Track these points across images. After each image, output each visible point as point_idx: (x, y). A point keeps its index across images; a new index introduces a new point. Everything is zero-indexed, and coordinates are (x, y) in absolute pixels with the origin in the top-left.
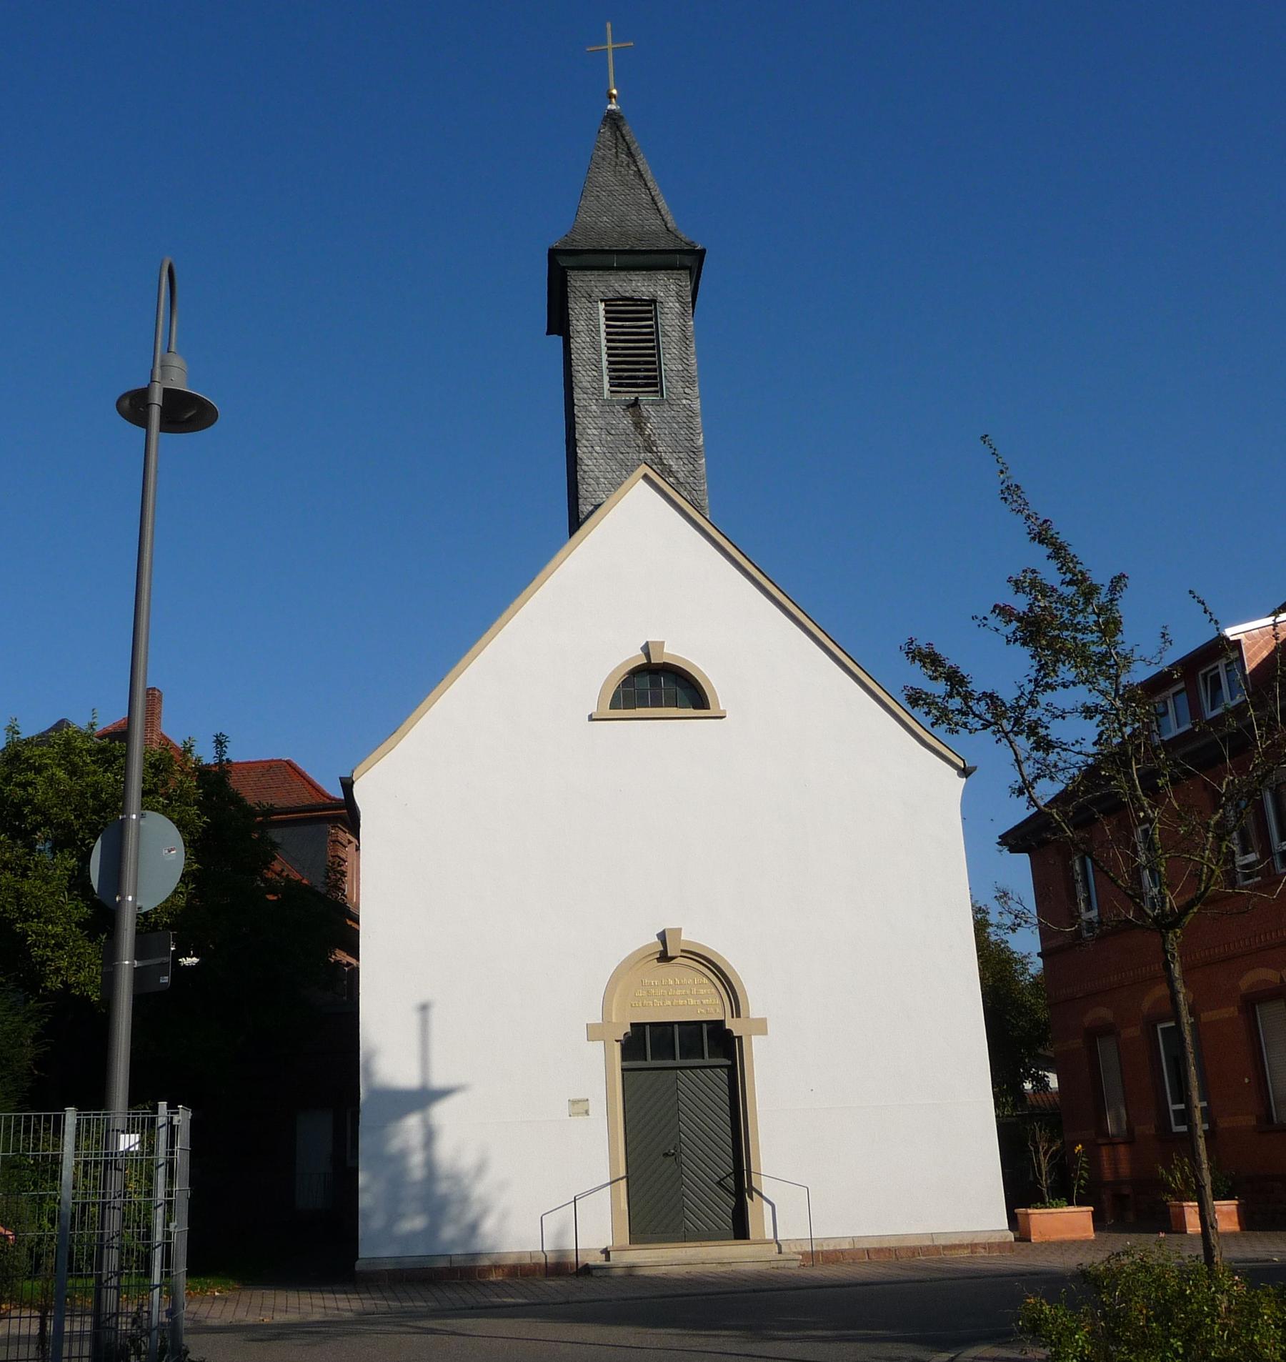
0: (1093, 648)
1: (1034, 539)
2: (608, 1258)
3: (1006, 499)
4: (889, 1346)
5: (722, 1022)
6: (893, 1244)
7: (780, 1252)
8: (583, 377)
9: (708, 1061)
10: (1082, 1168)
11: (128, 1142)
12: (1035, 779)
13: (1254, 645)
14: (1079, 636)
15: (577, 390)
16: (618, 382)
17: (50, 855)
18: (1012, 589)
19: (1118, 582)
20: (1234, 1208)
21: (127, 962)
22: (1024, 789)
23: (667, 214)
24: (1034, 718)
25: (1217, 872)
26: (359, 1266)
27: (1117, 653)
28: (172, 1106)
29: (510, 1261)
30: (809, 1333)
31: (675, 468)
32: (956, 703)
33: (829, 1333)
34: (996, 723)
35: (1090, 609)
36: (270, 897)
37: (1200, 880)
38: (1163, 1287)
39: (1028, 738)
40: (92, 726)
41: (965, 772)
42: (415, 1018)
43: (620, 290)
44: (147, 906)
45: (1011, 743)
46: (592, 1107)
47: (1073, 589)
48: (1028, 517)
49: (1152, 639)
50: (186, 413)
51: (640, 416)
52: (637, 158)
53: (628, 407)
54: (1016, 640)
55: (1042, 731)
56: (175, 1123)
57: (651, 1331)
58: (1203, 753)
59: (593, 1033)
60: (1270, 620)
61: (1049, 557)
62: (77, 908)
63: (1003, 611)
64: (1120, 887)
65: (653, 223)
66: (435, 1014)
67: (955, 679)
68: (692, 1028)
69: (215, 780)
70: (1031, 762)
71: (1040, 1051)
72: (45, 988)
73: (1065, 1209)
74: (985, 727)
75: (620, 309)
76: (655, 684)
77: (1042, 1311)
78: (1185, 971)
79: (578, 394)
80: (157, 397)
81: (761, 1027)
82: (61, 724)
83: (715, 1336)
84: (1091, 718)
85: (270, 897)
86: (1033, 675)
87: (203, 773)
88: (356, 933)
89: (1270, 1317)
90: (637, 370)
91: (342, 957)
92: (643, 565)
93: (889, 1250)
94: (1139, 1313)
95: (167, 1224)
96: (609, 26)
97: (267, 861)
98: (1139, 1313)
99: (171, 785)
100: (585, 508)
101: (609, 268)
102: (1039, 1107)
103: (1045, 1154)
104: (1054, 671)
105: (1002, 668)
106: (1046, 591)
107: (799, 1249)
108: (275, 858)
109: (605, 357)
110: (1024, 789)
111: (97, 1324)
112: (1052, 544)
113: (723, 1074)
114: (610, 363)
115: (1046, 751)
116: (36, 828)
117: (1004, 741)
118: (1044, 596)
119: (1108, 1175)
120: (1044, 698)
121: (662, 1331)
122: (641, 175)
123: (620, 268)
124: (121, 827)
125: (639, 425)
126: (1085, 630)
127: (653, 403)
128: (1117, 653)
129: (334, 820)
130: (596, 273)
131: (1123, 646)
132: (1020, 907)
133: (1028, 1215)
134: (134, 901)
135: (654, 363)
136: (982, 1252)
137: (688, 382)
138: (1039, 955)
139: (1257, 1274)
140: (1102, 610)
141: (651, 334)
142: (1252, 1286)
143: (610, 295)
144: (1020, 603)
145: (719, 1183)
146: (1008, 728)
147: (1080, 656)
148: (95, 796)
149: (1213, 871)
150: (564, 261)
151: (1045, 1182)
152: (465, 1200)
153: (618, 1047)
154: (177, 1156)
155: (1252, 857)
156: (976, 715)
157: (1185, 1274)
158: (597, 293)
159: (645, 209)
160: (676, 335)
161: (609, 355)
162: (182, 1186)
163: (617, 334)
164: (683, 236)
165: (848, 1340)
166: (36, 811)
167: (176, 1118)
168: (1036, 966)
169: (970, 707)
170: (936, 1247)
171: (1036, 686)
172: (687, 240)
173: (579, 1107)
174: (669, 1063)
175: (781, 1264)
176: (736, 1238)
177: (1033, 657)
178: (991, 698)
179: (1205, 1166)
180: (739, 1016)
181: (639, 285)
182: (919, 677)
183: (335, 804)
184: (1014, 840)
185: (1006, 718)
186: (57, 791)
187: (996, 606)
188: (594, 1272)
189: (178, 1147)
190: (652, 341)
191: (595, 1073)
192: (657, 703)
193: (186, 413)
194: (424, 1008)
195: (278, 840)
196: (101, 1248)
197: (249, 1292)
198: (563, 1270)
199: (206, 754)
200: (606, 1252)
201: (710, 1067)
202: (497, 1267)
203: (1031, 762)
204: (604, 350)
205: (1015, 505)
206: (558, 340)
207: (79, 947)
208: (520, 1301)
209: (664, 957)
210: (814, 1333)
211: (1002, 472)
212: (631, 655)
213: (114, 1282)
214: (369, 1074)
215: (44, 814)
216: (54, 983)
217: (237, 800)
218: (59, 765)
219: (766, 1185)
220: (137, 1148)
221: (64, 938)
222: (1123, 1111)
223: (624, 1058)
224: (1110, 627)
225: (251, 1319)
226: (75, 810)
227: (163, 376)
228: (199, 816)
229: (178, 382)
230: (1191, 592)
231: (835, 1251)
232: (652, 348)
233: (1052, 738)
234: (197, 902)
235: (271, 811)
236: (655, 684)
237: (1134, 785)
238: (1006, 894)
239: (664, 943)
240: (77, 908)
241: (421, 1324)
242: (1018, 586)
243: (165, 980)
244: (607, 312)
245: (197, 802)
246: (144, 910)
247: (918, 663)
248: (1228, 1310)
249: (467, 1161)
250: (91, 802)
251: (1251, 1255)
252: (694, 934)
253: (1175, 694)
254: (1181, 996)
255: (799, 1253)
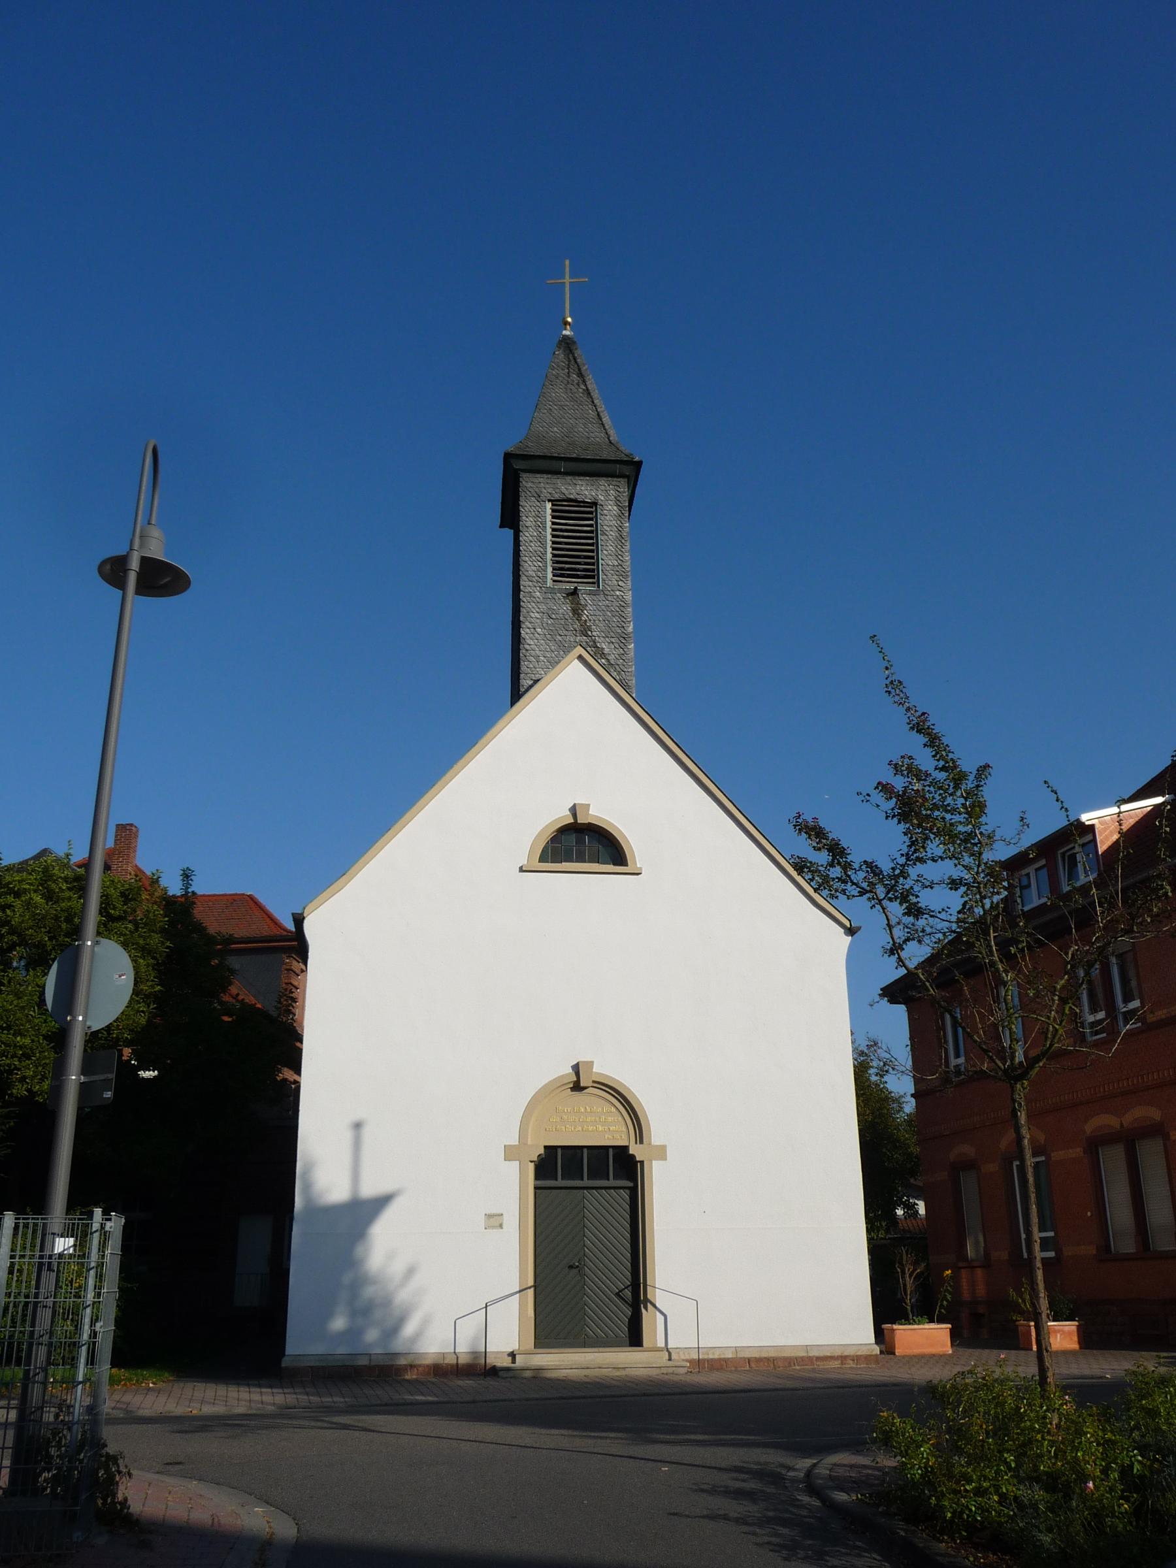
0: (961, 828)
1: (912, 728)
2: (514, 1361)
3: (889, 692)
4: (758, 1451)
5: (626, 1148)
6: (772, 1354)
7: (670, 1359)
8: (529, 566)
9: (612, 1182)
10: (947, 1290)
11: (63, 1245)
12: (905, 941)
13: (1105, 830)
14: (948, 816)
15: (523, 578)
16: (560, 572)
17: (24, 973)
18: (892, 771)
19: (983, 770)
20: (1074, 1328)
21: (74, 1077)
22: (895, 949)
23: (610, 428)
24: (907, 887)
25: (1061, 1031)
26: (285, 1362)
27: (981, 833)
28: (106, 1213)
29: (428, 1361)
30: (687, 1437)
31: (606, 651)
32: (836, 872)
33: (706, 1437)
34: (871, 891)
35: (959, 793)
36: (226, 1019)
37: (1046, 1038)
38: (1002, 1405)
39: (901, 904)
40: (68, 855)
41: (851, 931)
42: (348, 1135)
43: (566, 492)
44: (96, 1027)
45: (884, 909)
46: (506, 1221)
47: (943, 775)
48: (908, 709)
49: (1014, 822)
50: (160, 579)
51: (578, 603)
52: (587, 379)
53: (568, 595)
54: (894, 816)
55: (913, 899)
56: (107, 1228)
57: (543, 1431)
58: (1053, 925)
59: (510, 1153)
60: (1115, 810)
61: (925, 745)
62: (45, 1022)
63: (885, 789)
64: (975, 1041)
65: (597, 436)
66: (367, 1133)
67: (837, 851)
68: (599, 1153)
69: (181, 911)
70: (901, 927)
71: (912, 1181)
72: (11, 1095)
73: (927, 1326)
74: (861, 894)
75: (566, 509)
76: (580, 842)
77: (893, 1424)
78: (1029, 1116)
79: (524, 582)
80: (135, 564)
81: (661, 1153)
82: (45, 852)
83: (601, 1438)
84: (956, 889)
85: (226, 1019)
86: (905, 850)
87: (169, 903)
88: (299, 1051)
89: (1092, 1435)
90: (577, 563)
91: (288, 1074)
92: (572, 736)
93: (768, 1359)
94: (979, 1427)
95: (93, 1322)
96: (567, 262)
97: (224, 985)
98: (979, 1427)
99: (139, 915)
100: (525, 682)
101: (557, 473)
102: (910, 1232)
103: (910, 1276)
104: (923, 847)
105: (878, 840)
106: (919, 775)
107: (687, 1357)
108: (231, 983)
109: (549, 550)
110: (895, 949)
111: (22, 1416)
112: (929, 734)
113: (625, 1195)
114: (554, 556)
115: (917, 917)
116: (12, 947)
117: (878, 907)
118: (919, 780)
119: (966, 1295)
120: (913, 872)
121: (556, 1432)
122: (589, 394)
123: (567, 473)
124: (77, 952)
125: (577, 611)
126: (953, 811)
127: (590, 593)
128: (981, 833)
129: (288, 951)
130: (545, 476)
131: (985, 827)
132: (888, 1056)
133: (893, 1330)
134: (84, 1020)
135: (592, 558)
136: (851, 1364)
137: (622, 576)
138: (912, 1095)
139: (1086, 1392)
140: (969, 794)
141: (591, 532)
142: (1080, 1405)
143: (557, 496)
144: (899, 783)
145: (617, 1295)
146: (882, 896)
147: (948, 834)
148: (69, 920)
149: (1056, 1030)
150: (517, 464)
151: (909, 1301)
152: (387, 1302)
153: (531, 1167)
154: (107, 1259)
155: (1101, 1015)
156: (853, 884)
157: (1022, 1389)
158: (545, 494)
159: (591, 423)
160: (613, 534)
161: (554, 549)
162: (111, 1288)
163: (561, 530)
164: (622, 448)
165: (723, 1445)
166: (12, 931)
167: (108, 1224)
168: (910, 1106)
169: (849, 876)
170: (810, 1359)
171: (908, 859)
172: (627, 452)
173: (494, 1221)
174: (577, 1183)
175: (670, 1370)
176: (631, 1345)
177: (905, 834)
178: (871, 867)
179: (1042, 1295)
180: (641, 1142)
181: (583, 489)
182: (804, 847)
183: (287, 937)
184: (893, 993)
185: (889, 886)
186: (34, 915)
187: (879, 783)
188: (501, 1373)
189: (108, 1252)
190: (592, 538)
191: (510, 1191)
192: (581, 859)
193: (160, 579)
194: (358, 1126)
195: (237, 967)
196: (30, 1345)
197: (182, 1385)
198: (479, 1370)
199: (175, 888)
200: (513, 1355)
201: (614, 1188)
202: (412, 1366)
203: (901, 927)
204: (549, 544)
205: (897, 698)
206: (509, 532)
207: (45, 1058)
208: (430, 1399)
209: (577, 1087)
210: (693, 1437)
211: (887, 668)
212: (560, 815)
213: (40, 1378)
214: (308, 1187)
215: (19, 935)
216: (19, 1090)
217: (199, 928)
218: (35, 891)
219: (659, 1297)
220: (87, 1248)
221: (31, 1049)
222: (981, 1238)
223: (537, 1177)
224: (976, 809)
225: (179, 1411)
226: (49, 932)
227: (142, 546)
228: (163, 943)
229: (156, 550)
230: (1046, 782)
231: (720, 1359)
232: (592, 545)
233: (922, 905)
234: (157, 1020)
235: (230, 940)
236: (580, 842)
237: (991, 951)
238: (876, 1044)
239: (577, 1074)
240: (45, 1022)
241: (336, 1419)
242: (897, 768)
243: (108, 1095)
244: (553, 511)
245: (163, 931)
246: (94, 1029)
247: (804, 835)
248: (1058, 1426)
249: (397, 1268)
250: (64, 926)
251: (1087, 1372)
252: (605, 1067)
253: (1037, 870)
254: (1026, 1141)
255: (687, 1361)
